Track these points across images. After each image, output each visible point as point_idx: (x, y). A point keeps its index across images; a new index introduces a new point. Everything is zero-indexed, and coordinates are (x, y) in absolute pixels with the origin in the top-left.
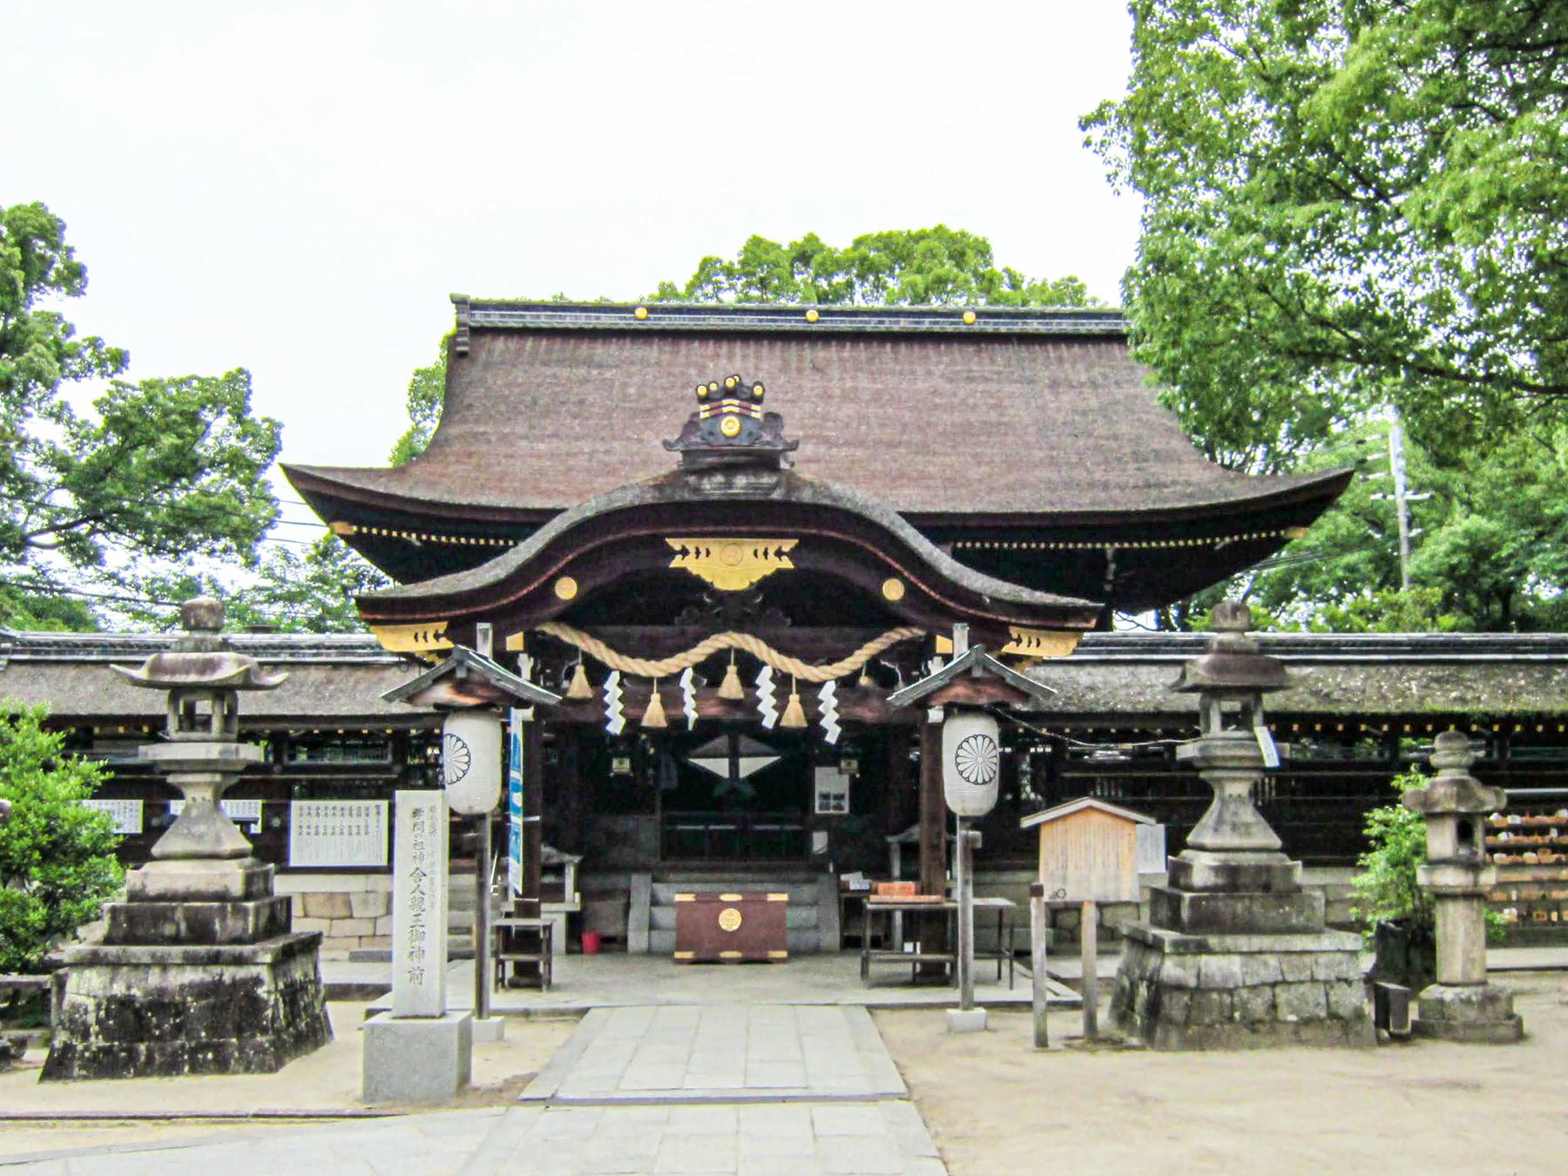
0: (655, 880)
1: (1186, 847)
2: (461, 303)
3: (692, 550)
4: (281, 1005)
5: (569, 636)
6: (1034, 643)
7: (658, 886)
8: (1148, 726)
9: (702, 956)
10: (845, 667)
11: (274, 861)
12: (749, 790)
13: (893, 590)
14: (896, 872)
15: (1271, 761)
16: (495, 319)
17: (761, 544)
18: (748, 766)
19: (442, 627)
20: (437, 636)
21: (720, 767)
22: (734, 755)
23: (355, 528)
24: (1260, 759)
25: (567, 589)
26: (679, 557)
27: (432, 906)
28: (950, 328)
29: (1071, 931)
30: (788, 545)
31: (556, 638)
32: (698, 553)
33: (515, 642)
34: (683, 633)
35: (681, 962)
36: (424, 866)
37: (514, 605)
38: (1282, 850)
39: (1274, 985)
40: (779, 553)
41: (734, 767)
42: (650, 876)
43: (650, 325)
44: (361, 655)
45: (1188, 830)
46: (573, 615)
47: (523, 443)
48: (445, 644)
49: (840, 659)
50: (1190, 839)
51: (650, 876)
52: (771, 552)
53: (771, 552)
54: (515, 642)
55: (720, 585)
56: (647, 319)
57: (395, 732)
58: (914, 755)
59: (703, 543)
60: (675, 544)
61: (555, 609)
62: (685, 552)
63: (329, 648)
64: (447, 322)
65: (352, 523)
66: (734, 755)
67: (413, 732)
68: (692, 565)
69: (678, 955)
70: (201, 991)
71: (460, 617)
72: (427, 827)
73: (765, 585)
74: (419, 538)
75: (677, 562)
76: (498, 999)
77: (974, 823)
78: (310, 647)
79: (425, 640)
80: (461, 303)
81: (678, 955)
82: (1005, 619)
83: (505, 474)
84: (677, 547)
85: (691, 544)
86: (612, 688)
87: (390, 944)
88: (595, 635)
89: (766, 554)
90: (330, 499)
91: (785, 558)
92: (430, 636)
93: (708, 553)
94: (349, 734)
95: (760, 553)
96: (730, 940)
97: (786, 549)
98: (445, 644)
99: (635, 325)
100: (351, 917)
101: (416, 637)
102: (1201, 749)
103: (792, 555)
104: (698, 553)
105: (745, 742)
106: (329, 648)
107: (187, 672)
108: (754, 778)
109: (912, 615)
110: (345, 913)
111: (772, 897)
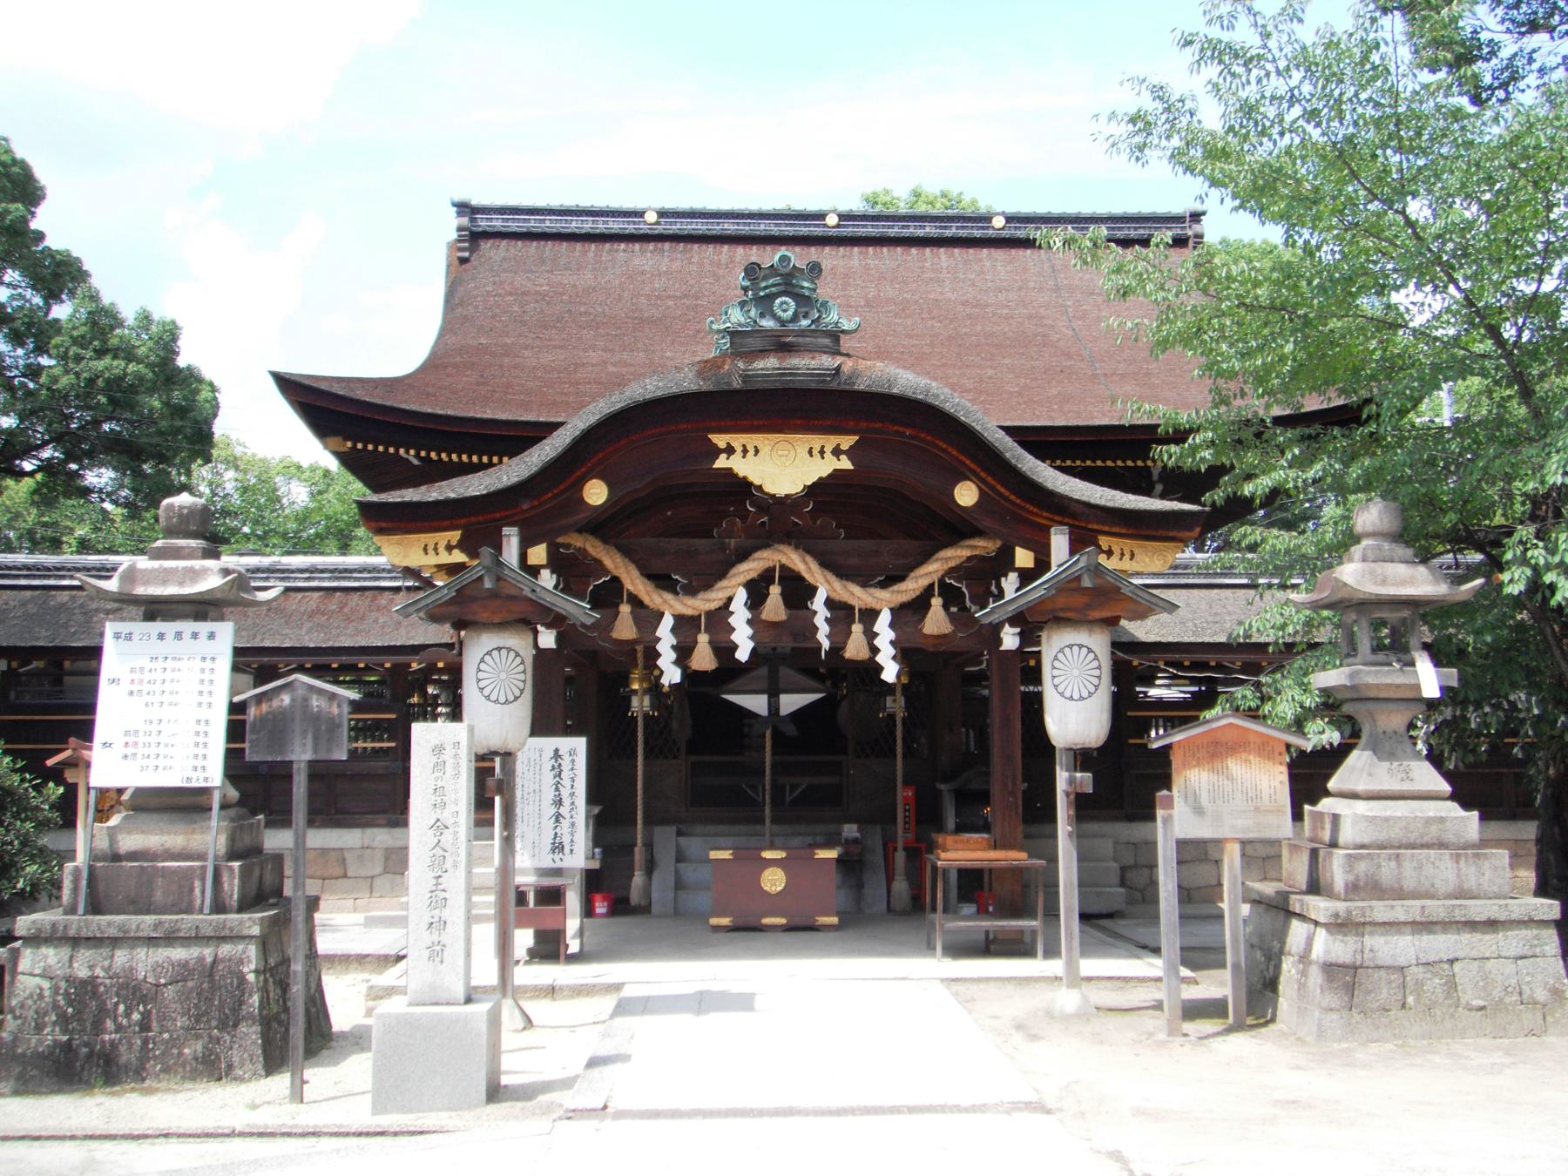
0: (680, 834)
1: (1327, 794)
2: (463, 208)
3: (739, 449)
4: (271, 987)
5: (595, 548)
6: (1127, 556)
7: (682, 840)
8: (1226, 660)
9: (798, 921)
10: (911, 587)
11: (262, 811)
12: (791, 730)
13: (966, 495)
14: (951, 823)
15: (1431, 690)
16: (497, 223)
17: (816, 441)
18: (791, 702)
19: (455, 536)
20: (449, 548)
21: (756, 703)
22: (773, 695)
23: (349, 444)
24: (1417, 687)
25: (596, 493)
26: (723, 456)
27: (455, 866)
28: (977, 233)
29: (1142, 891)
30: (847, 442)
31: (583, 551)
32: (745, 451)
33: (538, 554)
34: (723, 548)
35: (717, 929)
36: (447, 817)
37: (542, 505)
38: (1453, 797)
39: (1452, 962)
40: (837, 452)
41: (774, 707)
42: (674, 828)
43: (659, 229)
44: (356, 579)
45: (1328, 777)
46: (602, 525)
47: (527, 353)
48: (458, 557)
49: (902, 579)
50: (1332, 785)
51: (674, 828)
52: (828, 450)
53: (828, 450)
54: (538, 554)
55: (770, 488)
56: (657, 223)
57: (395, 666)
58: (986, 692)
59: (751, 440)
60: (720, 440)
61: (582, 516)
62: (730, 450)
63: (322, 571)
64: (449, 226)
65: (346, 439)
66: (773, 695)
67: (415, 666)
68: (742, 466)
69: (714, 921)
70: (183, 972)
71: (477, 523)
72: (448, 767)
73: (817, 490)
74: (417, 456)
75: (721, 462)
76: (529, 974)
77: (1083, 758)
78: (302, 571)
79: (430, 552)
80: (463, 208)
81: (714, 921)
82: (1096, 527)
83: (509, 385)
84: (722, 445)
85: (737, 440)
86: (665, 630)
87: (988, 782)
88: (627, 553)
89: (822, 452)
90: (322, 409)
91: (843, 457)
92: (441, 549)
93: (757, 451)
94: (345, 668)
95: (815, 452)
96: (775, 903)
97: (845, 447)
98: (458, 557)
99: (644, 229)
100: (345, 876)
101: (425, 550)
102: (1351, 676)
103: (850, 453)
104: (745, 451)
105: (786, 673)
106: (322, 571)
107: (164, 583)
108: (799, 715)
109: (986, 523)
110: (340, 872)
111: (714, 855)
